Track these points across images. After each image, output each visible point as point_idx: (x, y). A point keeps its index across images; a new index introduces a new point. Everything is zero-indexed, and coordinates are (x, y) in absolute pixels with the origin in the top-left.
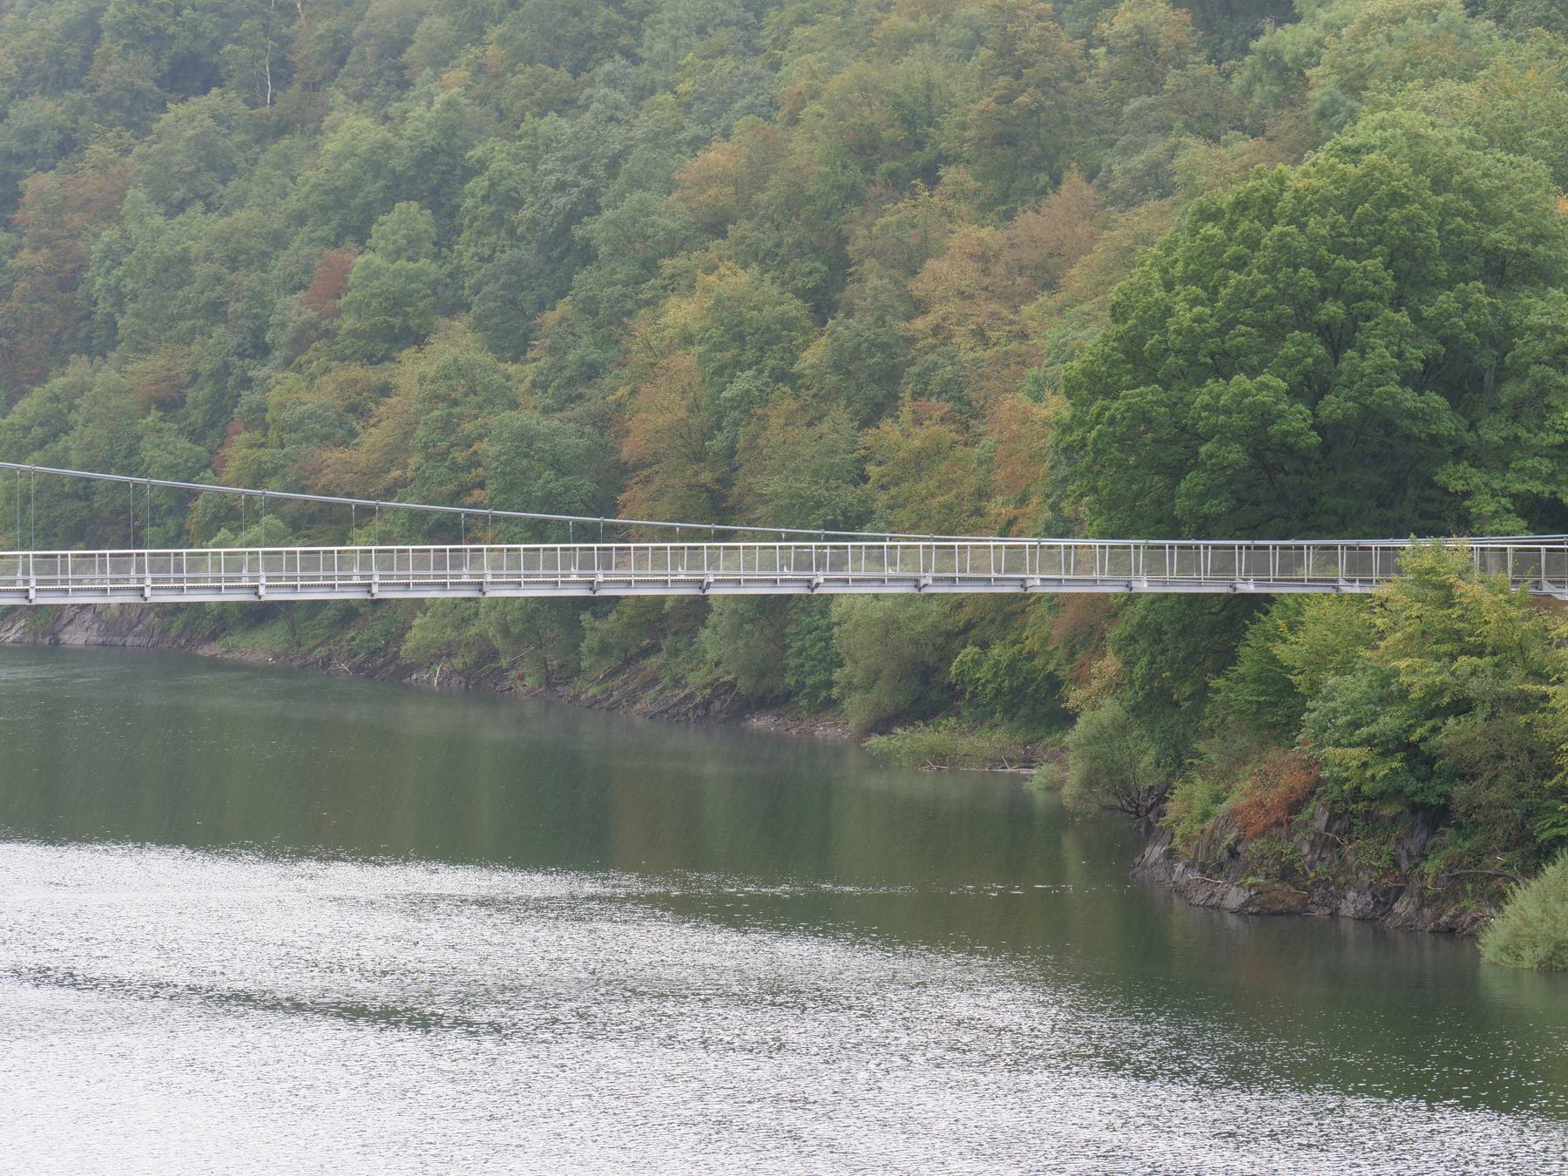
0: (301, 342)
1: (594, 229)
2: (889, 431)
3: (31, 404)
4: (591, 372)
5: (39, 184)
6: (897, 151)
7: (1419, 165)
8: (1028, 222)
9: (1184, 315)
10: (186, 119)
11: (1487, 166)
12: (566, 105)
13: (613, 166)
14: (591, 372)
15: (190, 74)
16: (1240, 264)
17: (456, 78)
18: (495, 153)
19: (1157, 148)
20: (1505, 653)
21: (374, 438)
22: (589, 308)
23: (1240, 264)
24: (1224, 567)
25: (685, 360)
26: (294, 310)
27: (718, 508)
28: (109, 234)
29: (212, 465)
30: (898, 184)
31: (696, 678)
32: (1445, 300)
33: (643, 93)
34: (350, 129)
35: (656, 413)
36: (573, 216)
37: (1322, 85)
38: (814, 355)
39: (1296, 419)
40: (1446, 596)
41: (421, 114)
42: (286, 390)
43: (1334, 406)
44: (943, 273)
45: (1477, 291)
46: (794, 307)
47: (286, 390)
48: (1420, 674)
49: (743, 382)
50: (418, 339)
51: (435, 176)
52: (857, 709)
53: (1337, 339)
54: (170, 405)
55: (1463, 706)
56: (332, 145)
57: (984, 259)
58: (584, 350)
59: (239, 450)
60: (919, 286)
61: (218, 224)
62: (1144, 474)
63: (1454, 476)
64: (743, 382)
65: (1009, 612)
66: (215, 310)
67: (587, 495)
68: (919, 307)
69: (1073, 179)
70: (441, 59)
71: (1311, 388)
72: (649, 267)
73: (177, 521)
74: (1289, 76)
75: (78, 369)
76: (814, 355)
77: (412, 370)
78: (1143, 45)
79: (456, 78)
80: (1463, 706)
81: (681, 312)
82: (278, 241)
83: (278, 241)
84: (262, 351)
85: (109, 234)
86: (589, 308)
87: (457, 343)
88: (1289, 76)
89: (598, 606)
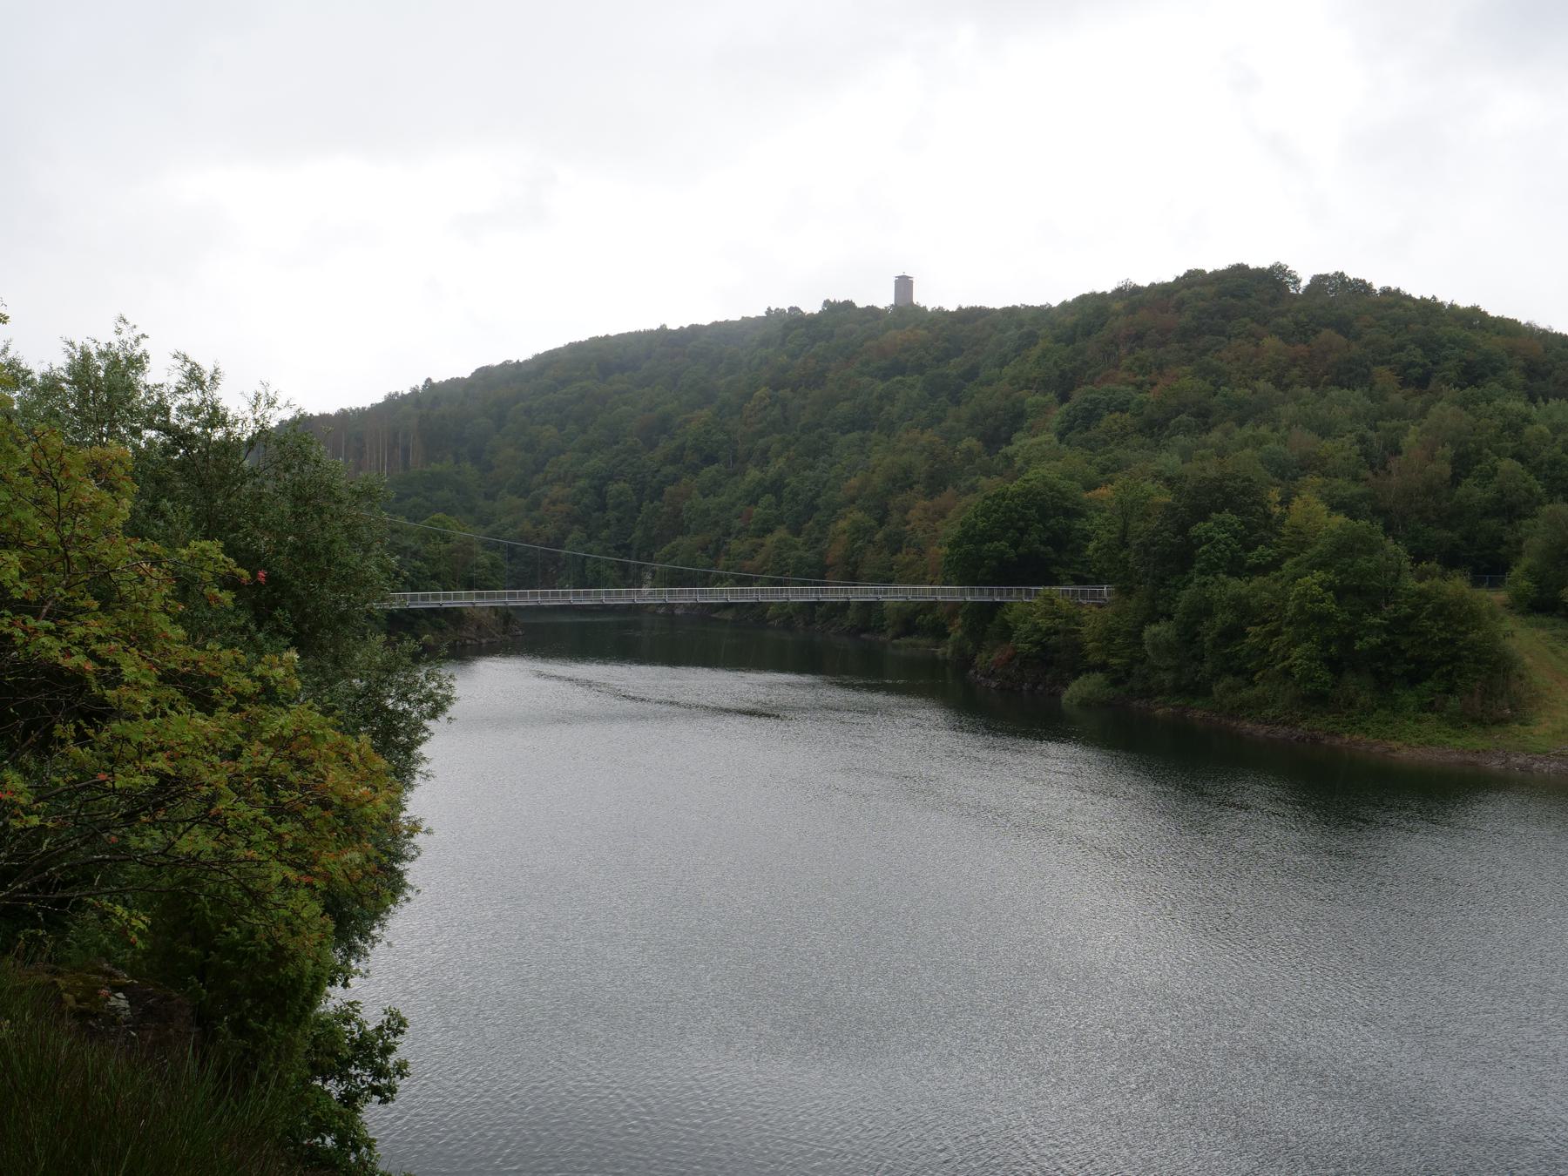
0: (739, 532)
1: (819, 501)
2: (899, 556)
3: (665, 549)
4: (818, 541)
5: (669, 489)
6: (902, 481)
7: (1045, 484)
8: (937, 499)
9: (981, 525)
10: (709, 472)
11: (1064, 484)
12: (812, 467)
13: (825, 485)
14: (818, 541)
15: (710, 459)
16: (996, 511)
17: (782, 461)
18: (792, 480)
19: (974, 479)
20: (1069, 618)
21: (759, 558)
22: (818, 523)
23: (996, 511)
24: (991, 593)
25: (844, 537)
26: (738, 524)
27: (853, 577)
28: (688, 503)
29: (715, 565)
30: (902, 489)
31: (847, 624)
32: (1052, 521)
33: (832, 465)
34: (753, 474)
35: (836, 551)
36: (813, 498)
37: (1019, 462)
38: (879, 536)
39: (1012, 553)
40: (1052, 602)
41: (772, 471)
42: (735, 545)
43: (1021, 550)
44: (914, 514)
45: (1061, 519)
46: (873, 523)
47: (735, 545)
48: (1044, 623)
49: (859, 543)
50: (771, 531)
51: (776, 487)
52: (890, 633)
53: (1022, 531)
54: (704, 549)
55: (1056, 633)
56: (748, 479)
57: (925, 510)
58: (816, 534)
59: (723, 561)
60: (908, 517)
61: (717, 500)
62: (968, 569)
63: (1055, 570)
64: (859, 543)
65: (932, 606)
66: (716, 523)
67: (818, 573)
68: (908, 523)
69: (950, 488)
70: (778, 455)
71: (1015, 544)
72: (834, 512)
73: (705, 580)
74: (1009, 459)
75: (679, 539)
76: (879, 536)
77: (770, 540)
78: (969, 451)
79: (782, 461)
80: (1056, 633)
81: (842, 524)
82: (734, 505)
83: (734, 505)
84: (730, 535)
85: (688, 503)
86: (818, 523)
87: (781, 533)
88: (1009, 459)
89: (820, 604)
